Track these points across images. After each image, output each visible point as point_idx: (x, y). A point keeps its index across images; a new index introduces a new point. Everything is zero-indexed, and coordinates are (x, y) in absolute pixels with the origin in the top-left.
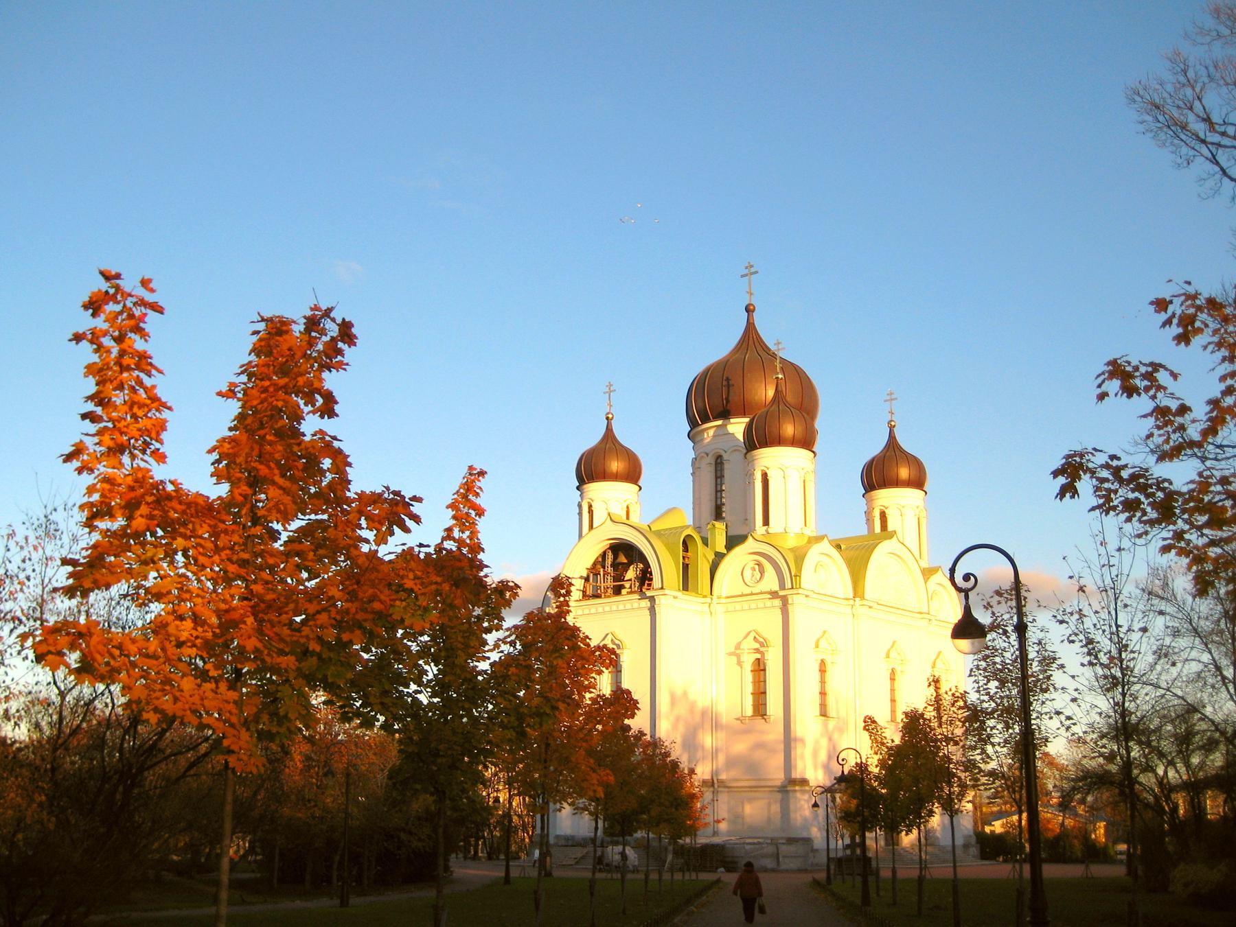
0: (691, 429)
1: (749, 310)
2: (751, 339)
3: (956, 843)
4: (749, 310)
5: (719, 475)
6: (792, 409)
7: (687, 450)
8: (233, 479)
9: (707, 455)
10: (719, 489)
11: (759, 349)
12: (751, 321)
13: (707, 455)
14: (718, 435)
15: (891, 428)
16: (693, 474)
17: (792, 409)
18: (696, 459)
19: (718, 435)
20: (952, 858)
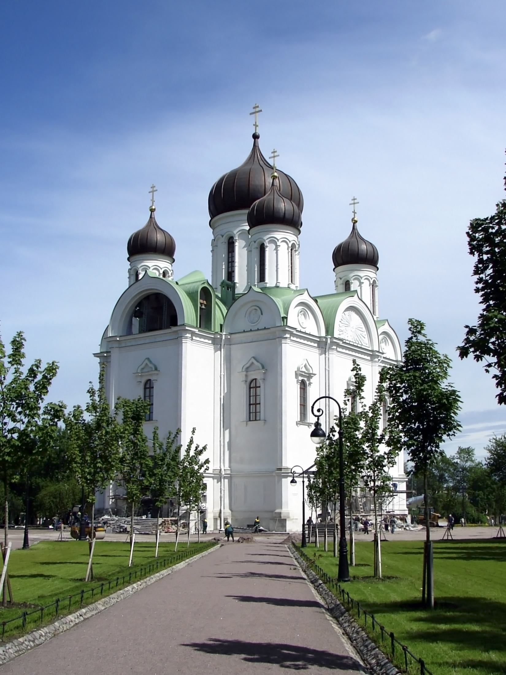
0: (212, 219)
1: (256, 137)
2: (256, 153)
3: (93, 573)
4: (256, 137)
5: (230, 250)
6: (284, 198)
7: (209, 234)
8: (83, 522)
9: (223, 236)
10: (230, 260)
11: (261, 162)
12: (257, 145)
13: (223, 236)
14: (136, 551)
15: (295, 307)
16: (212, 251)
17: (284, 198)
18: (214, 240)
19: (136, 551)
20: (4, 537)
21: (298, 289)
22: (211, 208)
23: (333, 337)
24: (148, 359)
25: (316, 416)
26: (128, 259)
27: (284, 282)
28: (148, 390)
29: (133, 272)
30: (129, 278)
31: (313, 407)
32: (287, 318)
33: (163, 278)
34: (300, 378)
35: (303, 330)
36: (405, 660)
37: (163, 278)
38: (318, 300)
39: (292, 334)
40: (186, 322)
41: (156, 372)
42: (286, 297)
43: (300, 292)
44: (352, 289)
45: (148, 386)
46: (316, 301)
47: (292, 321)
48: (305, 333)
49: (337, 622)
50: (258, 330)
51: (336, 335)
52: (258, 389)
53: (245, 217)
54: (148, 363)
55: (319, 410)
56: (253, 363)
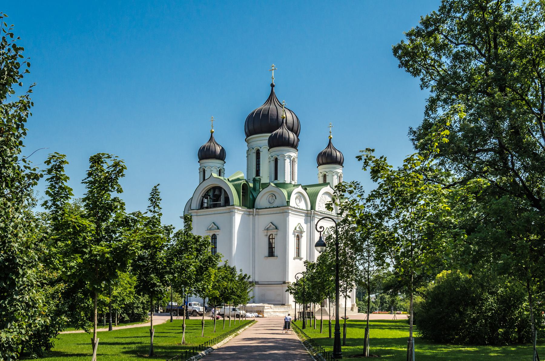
7: (245, 147)
16: (247, 157)
21: (296, 184)
22: (246, 131)
23: (315, 210)
24: (214, 223)
25: (318, 231)
26: (199, 162)
27: (288, 180)
28: (213, 240)
29: (201, 170)
30: (199, 173)
31: (316, 225)
32: (289, 202)
33: (220, 177)
34: (297, 234)
35: (298, 207)
36: (134, 338)
37: (220, 177)
38: (308, 188)
39: (292, 210)
40: (235, 204)
41: (218, 230)
42: (289, 189)
43: (297, 186)
44: (327, 182)
45: (213, 237)
46: (305, 189)
47: (293, 203)
48: (299, 209)
49: (136, 355)
50: (274, 207)
51: (317, 209)
52: (273, 240)
53: (268, 138)
54: (214, 225)
55: (321, 228)
56: (271, 226)
